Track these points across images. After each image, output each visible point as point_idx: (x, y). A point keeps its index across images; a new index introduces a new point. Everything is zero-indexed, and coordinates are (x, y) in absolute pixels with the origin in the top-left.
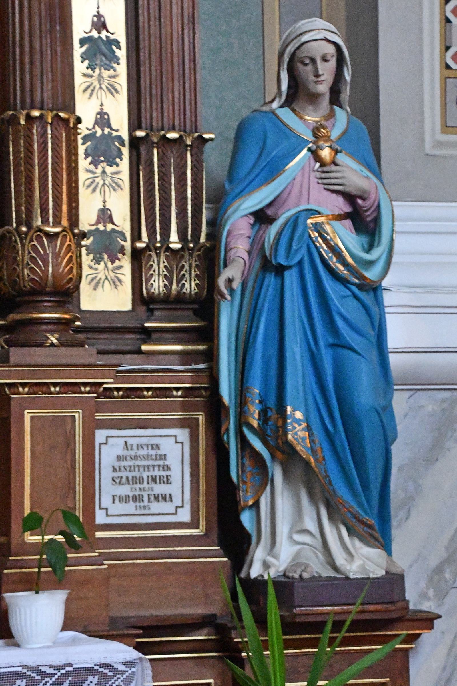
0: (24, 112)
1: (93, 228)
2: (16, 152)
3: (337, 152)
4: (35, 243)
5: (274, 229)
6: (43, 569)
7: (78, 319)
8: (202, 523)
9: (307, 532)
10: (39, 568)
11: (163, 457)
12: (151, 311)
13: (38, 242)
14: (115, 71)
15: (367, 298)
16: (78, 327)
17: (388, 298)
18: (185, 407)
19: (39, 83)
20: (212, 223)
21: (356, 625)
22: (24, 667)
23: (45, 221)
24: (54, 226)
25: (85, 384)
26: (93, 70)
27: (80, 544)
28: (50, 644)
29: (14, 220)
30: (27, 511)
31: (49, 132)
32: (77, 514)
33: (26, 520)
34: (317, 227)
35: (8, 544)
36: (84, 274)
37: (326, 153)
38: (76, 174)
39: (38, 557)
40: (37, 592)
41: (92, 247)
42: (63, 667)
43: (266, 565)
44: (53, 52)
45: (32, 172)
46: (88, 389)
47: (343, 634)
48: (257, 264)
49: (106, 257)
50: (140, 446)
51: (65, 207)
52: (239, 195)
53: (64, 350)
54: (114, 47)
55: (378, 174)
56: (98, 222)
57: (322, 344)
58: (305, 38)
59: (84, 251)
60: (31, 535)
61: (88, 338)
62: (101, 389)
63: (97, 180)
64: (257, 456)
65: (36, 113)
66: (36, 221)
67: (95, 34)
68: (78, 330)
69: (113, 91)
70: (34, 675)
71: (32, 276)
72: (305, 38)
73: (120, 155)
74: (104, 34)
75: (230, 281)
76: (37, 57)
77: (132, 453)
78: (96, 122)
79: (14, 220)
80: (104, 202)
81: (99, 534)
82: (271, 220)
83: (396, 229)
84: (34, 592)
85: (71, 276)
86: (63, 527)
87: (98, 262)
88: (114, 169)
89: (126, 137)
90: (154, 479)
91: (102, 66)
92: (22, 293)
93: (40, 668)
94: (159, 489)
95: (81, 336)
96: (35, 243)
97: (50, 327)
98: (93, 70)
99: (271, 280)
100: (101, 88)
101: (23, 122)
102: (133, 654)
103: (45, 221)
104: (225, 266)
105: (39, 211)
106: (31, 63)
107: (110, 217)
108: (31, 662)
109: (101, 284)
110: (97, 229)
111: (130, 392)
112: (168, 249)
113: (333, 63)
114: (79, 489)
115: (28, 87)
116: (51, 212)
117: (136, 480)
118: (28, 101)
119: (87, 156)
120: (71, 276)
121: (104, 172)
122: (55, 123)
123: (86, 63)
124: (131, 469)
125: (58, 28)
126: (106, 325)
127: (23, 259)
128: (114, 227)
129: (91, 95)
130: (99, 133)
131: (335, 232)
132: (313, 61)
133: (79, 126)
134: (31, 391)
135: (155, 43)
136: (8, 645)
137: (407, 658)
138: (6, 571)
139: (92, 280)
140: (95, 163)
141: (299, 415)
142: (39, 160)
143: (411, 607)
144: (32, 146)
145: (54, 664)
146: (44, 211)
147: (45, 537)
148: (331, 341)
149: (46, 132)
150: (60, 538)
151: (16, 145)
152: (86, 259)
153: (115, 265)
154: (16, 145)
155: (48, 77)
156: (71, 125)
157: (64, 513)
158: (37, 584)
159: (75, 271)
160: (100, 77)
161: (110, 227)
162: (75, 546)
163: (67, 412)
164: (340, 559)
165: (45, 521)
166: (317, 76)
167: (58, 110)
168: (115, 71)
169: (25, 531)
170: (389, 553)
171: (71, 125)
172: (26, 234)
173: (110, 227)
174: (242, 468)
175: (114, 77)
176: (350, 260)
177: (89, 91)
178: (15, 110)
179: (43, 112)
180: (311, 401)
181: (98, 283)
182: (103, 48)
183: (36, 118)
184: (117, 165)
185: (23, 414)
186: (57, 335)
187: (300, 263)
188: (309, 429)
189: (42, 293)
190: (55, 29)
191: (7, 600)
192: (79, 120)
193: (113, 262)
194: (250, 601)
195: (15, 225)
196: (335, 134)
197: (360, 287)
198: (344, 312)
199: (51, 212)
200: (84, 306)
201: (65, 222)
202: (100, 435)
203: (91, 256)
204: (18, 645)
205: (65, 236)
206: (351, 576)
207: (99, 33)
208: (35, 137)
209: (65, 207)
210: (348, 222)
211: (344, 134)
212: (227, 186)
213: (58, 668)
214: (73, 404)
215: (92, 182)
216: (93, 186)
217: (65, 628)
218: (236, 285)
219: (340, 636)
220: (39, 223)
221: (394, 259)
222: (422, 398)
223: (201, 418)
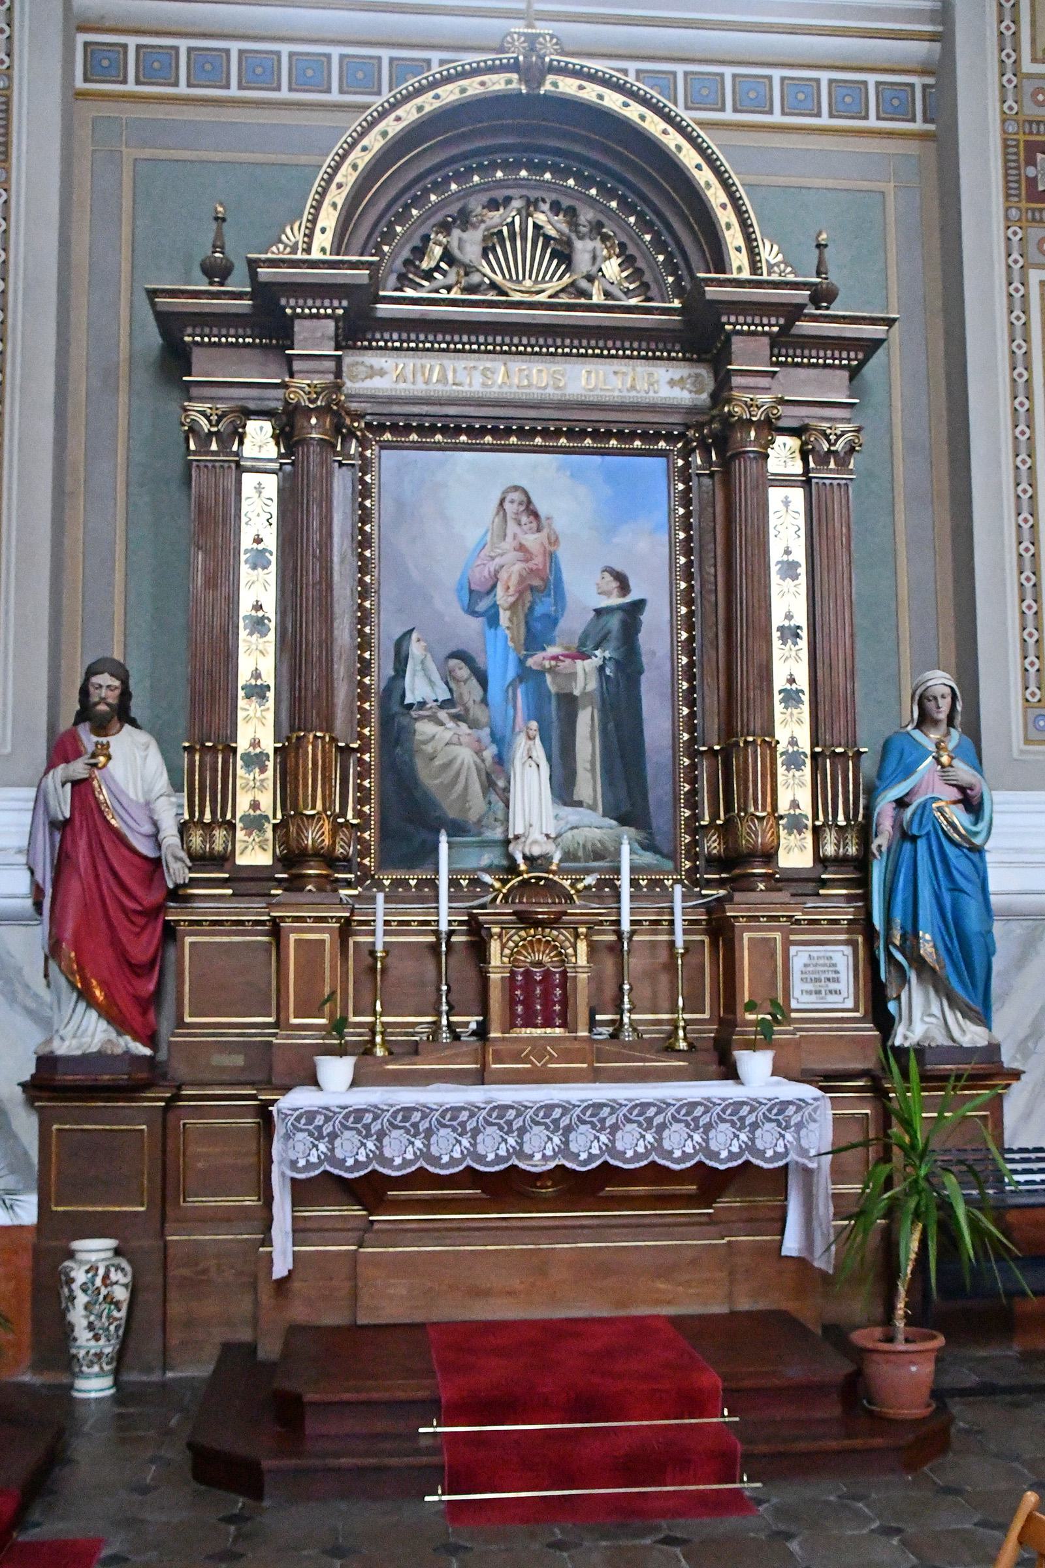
3: (952, 758)
5: (909, 811)
8: (862, 1009)
9: (934, 1016)
11: (834, 965)
12: (826, 867)
15: (975, 857)
17: (988, 857)
18: (848, 932)
20: (866, 808)
21: (972, 1077)
23: (756, 809)
30: (746, 1000)
33: (746, 1005)
34: (940, 809)
37: (945, 759)
43: (906, 1038)
44: (762, 700)
47: (963, 1083)
48: (898, 836)
50: (819, 958)
51: (769, 800)
52: (885, 789)
53: (768, 893)
55: (980, 771)
57: (943, 890)
58: (929, 683)
64: (899, 965)
65: (750, 739)
68: (778, 880)
72: (929, 683)
73: (804, 763)
75: (880, 846)
77: (814, 962)
81: (793, 1015)
82: (907, 805)
83: (30, 814)
86: (770, 1009)
88: (800, 773)
89: (808, 752)
90: (829, 980)
94: (833, 986)
95: (780, 885)
99: (907, 846)
102: (819, 1093)
103: (756, 809)
104: (876, 836)
111: (811, 922)
112: (837, 825)
113: (949, 699)
114: (780, 985)
117: (818, 980)
124: (813, 972)
131: (952, 813)
132: (935, 698)
135: (828, 692)
137: (1002, 1101)
140: (788, 770)
141: (928, 937)
143: (1005, 1065)
148: (950, 886)
150: (769, 1017)
152: (783, 833)
155: (758, 715)
157: (771, 1001)
160: (792, 714)
162: (778, 1023)
164: (956, 1033)
166: (938, 707)
170: (990, 1029)
174: (888, 972)
176: (963, 832)
180: (936, 930)
187: (928, 834)
188: (935, 946)
192: (778, 742)
194: (898, 1061)
196: (951, 746)
197: (970, 849)
198: (961, 868)
201: (769, 809)
202: (793, 950)
204: (742, 1084)
206: (965, 1045)
210: (961, 806)
211: (956, 747)
212: (877, 783)
213: (770, 1100)
217: (773, 1074)
218: (884, 849)
219: (960, 1084)
221: (993, 831)
222: (1014, 925)
223: (860, 939)
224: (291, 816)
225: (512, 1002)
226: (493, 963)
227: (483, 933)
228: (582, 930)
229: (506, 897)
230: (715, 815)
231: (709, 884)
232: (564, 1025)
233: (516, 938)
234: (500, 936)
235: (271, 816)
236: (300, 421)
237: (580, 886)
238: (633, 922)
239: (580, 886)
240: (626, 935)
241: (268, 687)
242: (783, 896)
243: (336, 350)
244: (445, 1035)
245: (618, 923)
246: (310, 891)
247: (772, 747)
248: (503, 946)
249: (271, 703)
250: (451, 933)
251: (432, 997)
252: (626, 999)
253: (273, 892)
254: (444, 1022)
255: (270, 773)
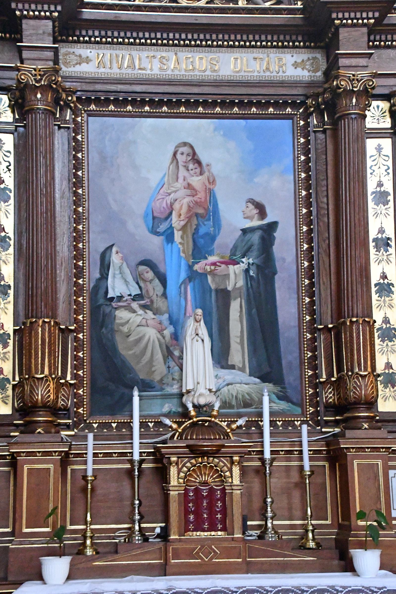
0: (349, 319)
1: (383, 372)
2: (345, 338)
4: (356, 380)
6: (368, 539)
7: (378, 416)
10: (366, 538)
13: (357, 380)
14: (392, 297)
16: (378, 420)
19: (356, 306)
22: (363, 587)
23: (360, 369)
24: (364, 371)
25: (383, 448)
26: (381, 297)
27: (385, 527)
28: (374, 576)
29: (345, 369)
30: (358, 510)
31: (361, 327)
32: (382, 512)
35: (350, 526)
36: (379, 394)
38: (374, 347)
39: (365, 532)
40: (366, 550)
41: (383, 381)
42: (382, 588)
45: (353, 347)
46: (384, 450)
49: (390, 385)
51: (369, 363)
53: (371, 431)
54: (391, 287)
56: (385, 369)
59: (379, 383)
60: (361, 521)
61: (383, 425)
62: (391, 450)
63: (384, 349)
65: (354, 319)
66: (356, 369)
67: (382, 281)
68: (377, 421)
69: (391, 307)
70: (368, 591)
71: (355, 396)
74: (386, 281)
76: (355, 294)
78: (383, 322)
79: (345, 369)
80: (388, 359)
84: (364, 550)
85: (373, 395)
86: (376, 518)
87: (386, 388)
91: (385, 296)
92: (350, 404)
93: (371, 588)
95: (379, 424)
96: (356, 380)
97: (364, 420)
98: (381, 297)
100: (385, 306)
101: (348, 324)
103: (360, 369)
105: (357, 364)
106: (352, 297)
107: (391, 366)
108: (366, 585)
109: (388, 399)
110: (385, 372)
114: (383, 499)
115: (350, 308)
116: (362, 365)
118: (351, 314)
119: (379, 338)
120: (373, 395)
121: (387, 345)
122: (363, 324)
123: (378, 294)
125: (364, 280)
126: (391, 419)
127: (350, 388)
128: (393, 371)
129: (380, 309)
130: (384, 327)
133: (375, 324)
134: (356, 451)
136: (355, 575)
138: (350, 539)
139: (384, 396)
140: (383, 341)
142: (356, 341)
144: (353, 335)
145: (377, 586)
146: (359, 365)
147: (368, 523)
149: (359, 327)
150: (375, 524)
151: (345, 334)
152: (380, 387)
153: (394, 389)
154: (345, 334)
156: (371, 324)
158: (365, 546)
159: (375, 393)
161: (391, 371)
162: (383, 528)
163: (374, 461)
165: (367, 515)
167: (365, 317)
168: (392, 297)
169: (357, 520)
171: (371, 324)
172: (351, 375)
173: (391, 371)
175: (392, 300)
177: (379, 307)
178: (345, 318)
179: (358, 319)
181: (386, 398)
182: (386, 287)
183: (355, 321)
184: (394, 342)
185: (353, 463)
186: (368, 424)
189: (360, 404)
190: (363, 280)
191: (352, 553)
192: (375, 322)
193: (393, 388)
195: (346, 372)
199: (362, 365)
200: (380, 409)
201: (369, 370)
203: (383, 385)
204: (359, 576)
205: (369, 376)
207: (384, 280)
208: (354, 330)
209: (369, 363)
213: (380, 589)
214: (377, 457)
215: (382, 350)
216: (383, 351)
217: (381, 568)
220: (357, 370)
224: (26, 379)
225: (187, 512)
226: (172, 484)
227: (165, 461)
228: (236, 458)
229: (181, 435)
230: (330, 374)
231: (327, 424)
232: (224, 529)
233: (188, 465)
234: (177, 464)
235: (11, 379)
236: (29, 96)
237: (234, 426)
238: (272, 452)
239: (234, 426)
240: (268, 462)
241: (9, 286)
242: (383, 433)
243: (54, 44)
244: (137, 538)
245: (262, 452)
246: (39, 433)
247: (371, 324)
248: (179, 471)
249: (11, 298)
250: (141, 462)
251: (128, 510)
252: (269, 509)
253: (12, 434)
254: (137, 528)
255: (10, 348)
